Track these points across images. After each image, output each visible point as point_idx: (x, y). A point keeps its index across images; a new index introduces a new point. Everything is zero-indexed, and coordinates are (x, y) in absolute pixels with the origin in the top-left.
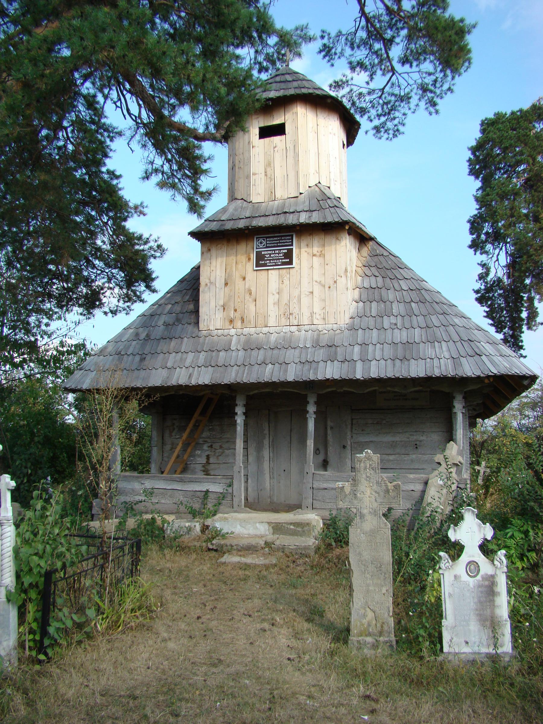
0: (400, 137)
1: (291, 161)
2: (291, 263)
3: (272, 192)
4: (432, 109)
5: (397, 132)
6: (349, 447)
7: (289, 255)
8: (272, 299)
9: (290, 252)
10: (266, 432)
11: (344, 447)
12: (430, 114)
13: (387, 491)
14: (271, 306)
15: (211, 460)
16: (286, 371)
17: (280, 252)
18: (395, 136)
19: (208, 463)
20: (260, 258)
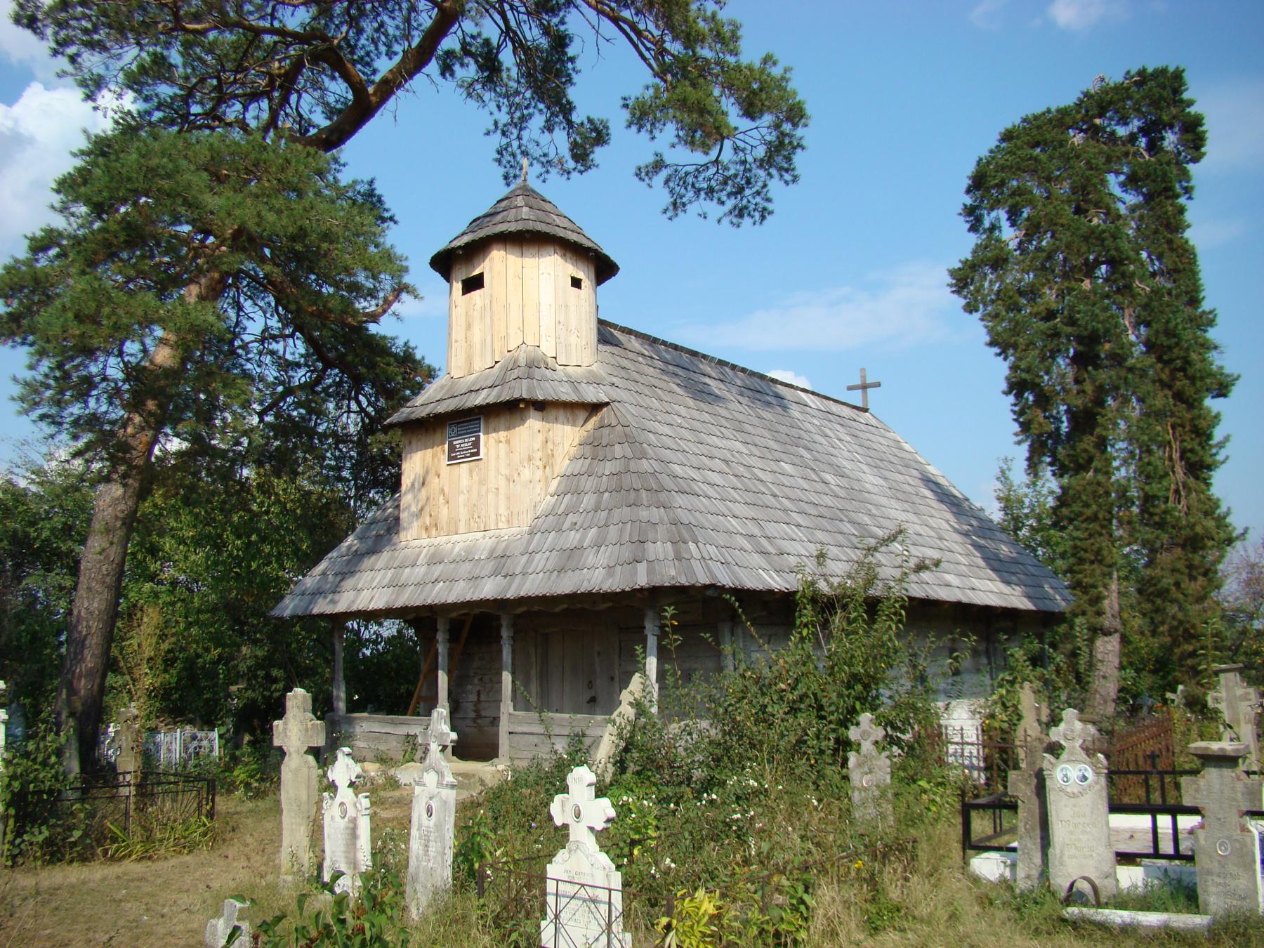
0: (769, 218)
1: (488, 320)
2: (477, 454)
3: (470, 364)
4: (787, 177)
5: (764, 214)
6: (617, 679)
7: (476, 444)
8: (462, 498)
9: (478, 438)
10: (533, 660)
11: (612, 679)
12: (787, 183)
13: (307, 730)
14: (462, 508)
15: (483, 698)
16: (635, 573)
17: (463, 443)
18: (763, 218)
19: (479, 701)
20: (452, 448)
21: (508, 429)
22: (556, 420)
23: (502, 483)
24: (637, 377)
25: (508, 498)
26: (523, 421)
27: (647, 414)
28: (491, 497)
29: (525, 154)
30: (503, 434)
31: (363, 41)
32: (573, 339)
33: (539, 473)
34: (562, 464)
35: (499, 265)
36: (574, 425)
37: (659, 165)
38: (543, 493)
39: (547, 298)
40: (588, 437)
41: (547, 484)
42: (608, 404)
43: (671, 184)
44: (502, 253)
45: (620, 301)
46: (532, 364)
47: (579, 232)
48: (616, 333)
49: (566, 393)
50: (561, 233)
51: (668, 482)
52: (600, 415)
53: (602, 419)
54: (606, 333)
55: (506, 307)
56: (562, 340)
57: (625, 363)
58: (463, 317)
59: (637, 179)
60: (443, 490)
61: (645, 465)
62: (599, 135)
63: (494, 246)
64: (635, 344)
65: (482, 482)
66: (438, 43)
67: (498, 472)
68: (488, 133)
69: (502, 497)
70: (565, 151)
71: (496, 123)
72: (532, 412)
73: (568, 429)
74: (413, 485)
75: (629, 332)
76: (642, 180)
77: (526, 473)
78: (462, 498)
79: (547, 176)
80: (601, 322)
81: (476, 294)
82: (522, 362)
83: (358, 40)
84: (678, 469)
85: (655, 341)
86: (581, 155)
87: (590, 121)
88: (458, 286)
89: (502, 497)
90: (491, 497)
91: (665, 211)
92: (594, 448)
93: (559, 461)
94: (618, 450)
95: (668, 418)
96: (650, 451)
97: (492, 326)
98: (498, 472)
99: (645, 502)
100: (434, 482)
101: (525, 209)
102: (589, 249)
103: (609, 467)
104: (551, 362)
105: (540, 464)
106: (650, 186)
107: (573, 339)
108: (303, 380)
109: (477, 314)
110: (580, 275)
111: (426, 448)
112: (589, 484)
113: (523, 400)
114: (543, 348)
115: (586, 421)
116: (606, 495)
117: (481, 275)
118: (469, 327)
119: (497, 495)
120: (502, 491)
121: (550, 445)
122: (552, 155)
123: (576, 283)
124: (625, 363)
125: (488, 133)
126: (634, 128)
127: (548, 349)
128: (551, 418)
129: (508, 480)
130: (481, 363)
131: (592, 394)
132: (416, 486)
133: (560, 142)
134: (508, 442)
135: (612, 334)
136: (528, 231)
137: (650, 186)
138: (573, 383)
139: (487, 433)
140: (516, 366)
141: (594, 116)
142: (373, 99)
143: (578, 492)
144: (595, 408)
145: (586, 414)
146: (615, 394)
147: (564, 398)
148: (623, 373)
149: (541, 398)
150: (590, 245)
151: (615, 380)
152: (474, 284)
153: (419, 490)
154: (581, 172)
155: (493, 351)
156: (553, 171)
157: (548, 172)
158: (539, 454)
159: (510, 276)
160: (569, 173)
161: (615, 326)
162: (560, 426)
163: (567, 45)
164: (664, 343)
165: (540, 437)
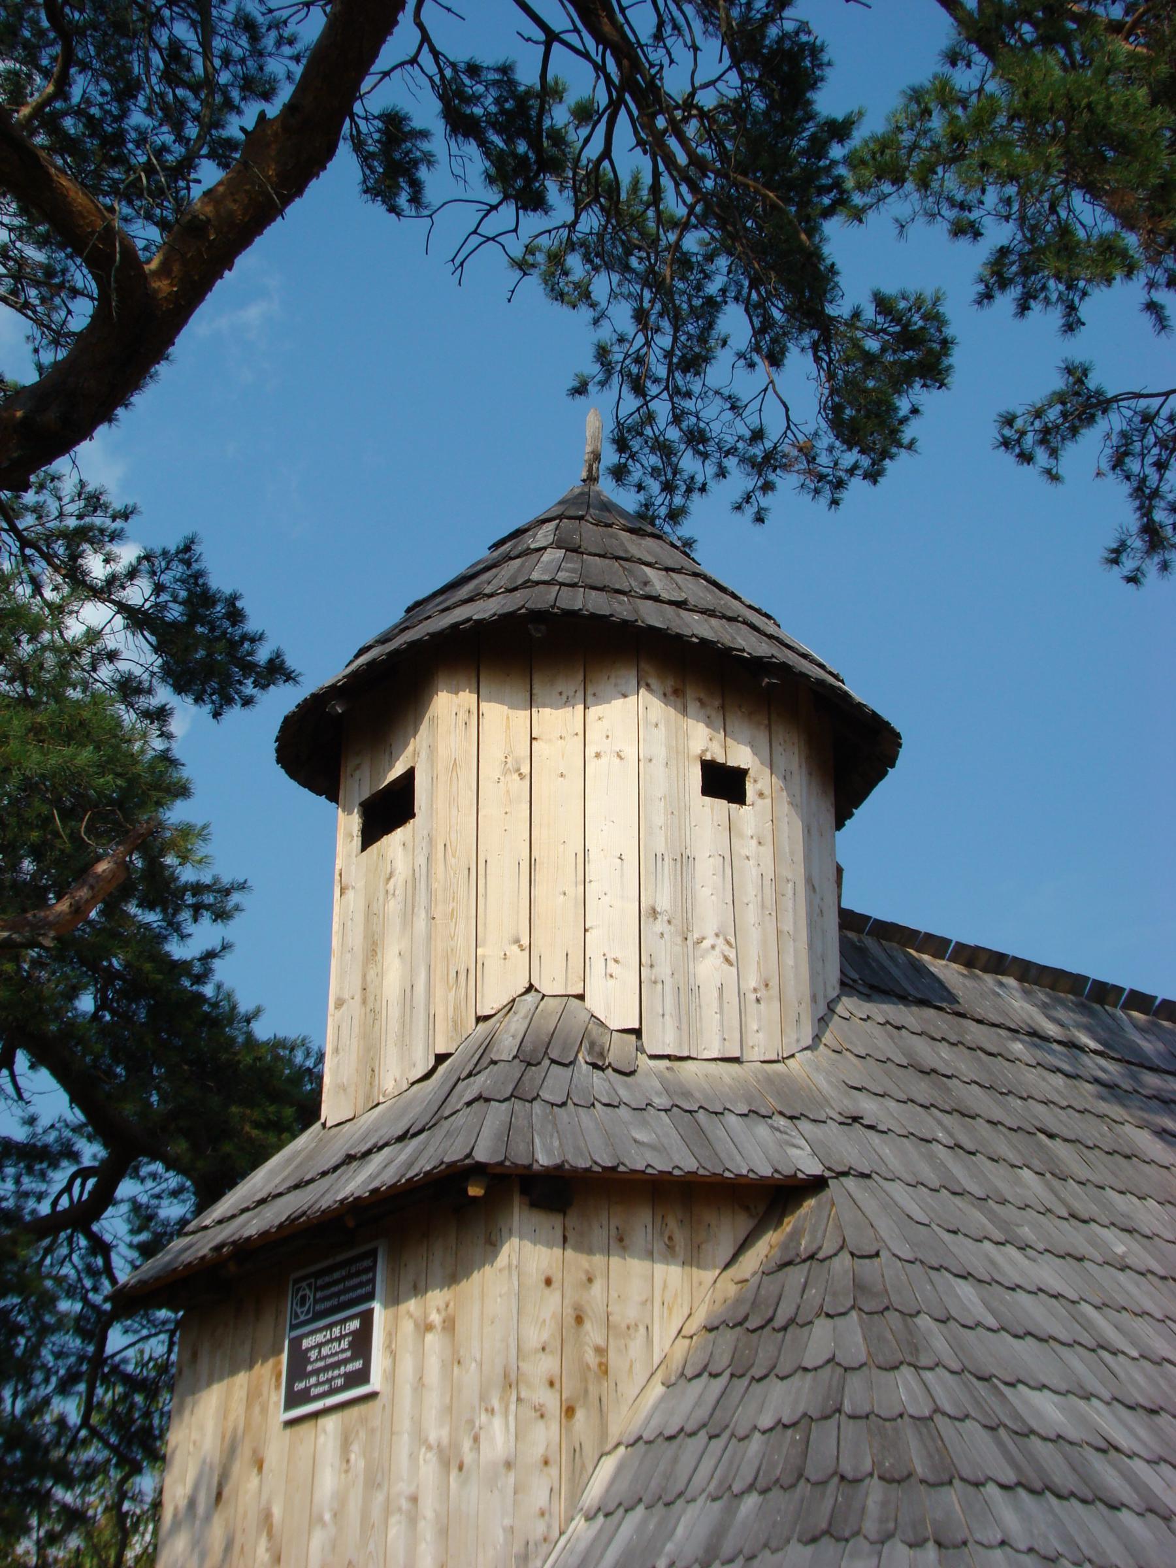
2: (362, 1377)
7: (361, 1343)
9: (367, 1318)
17: (325, 1342)
20: (298, 1367)
21: (453, 1278)
22: (621, 1243)
23: (429, 1468)
24: (976, 1099)
25: (444, 1532)
26: (493, 1245)
27: (977, 1219)
28: (396, 1529)
29: (697, 438)
30: (437, 1298)
31: (137, 118)
32: (709, 970)
33: (544, 1436)
34: (639, 1398)
35: (461, 736)
36: (693, 1258)
37: (1081, 404)
38: (560, 1508)
39: (613, 836)
40: (738, 1301)
41: (578, 1480)
42: (817, 1184)
43: (1134, 465)
44: (467, 698)
45: (912, 856)
46: (535, 1055)
47: (756, 620)
48: (941, 968)
49: (654, 1147)
50: (653, 616)
51: (978, 1450)
52: (790, 1223)
53: (795, 1235)
54: (873, 960)
55: (477, 869)
56: (663, 970)
57: (942, 1057)
58: (360, 918)
59: (1008, 459)
60: (267, 1516)
61: (904, 1391)
62: (917, 348)
63: (441, 681)
64: (1018, 1004)
65: (375, 1479)
66: (352, 93)
67: (419, 1438)
68: (580, 390)
69: (427, 1529)
70: (809, 415)
71: (602, 353)
72: (519, 1216)
73: (670, 1276)
74: (192, 1503)
75: (974, 958)
76: (1026, 458)
77: (498, 1437)
78: (318, 1540)
79: (765, 501)
80: (850, 921)
81: (395, 841)
82: (506, 1047)
83: (124, 114)
84: (1048, 1410)
85: (1095, 995)
86: (868, 424)
87: (883, 304)
88: (350, 823)
89: (427, 1529)
90: (396, 1529)
91: (1115, 556)
92: (747, 1339)
93: (630, 1390)
94: (820, 1341)
95: (1074, 1237)
96: (938, 1341)
97: (429, 938)
98: (419, 1438)
99: (871, 1527)
100: (247, 1488)
101: (553, 556)
102: (759, 665)
103: (779, 1401)
104: (619, 1050)
105: (551, 1401)
106: (1053, 476)
107: (709, 970)
108: (64, 1202)
109: (393, 906)
110: (740, 755)
111: (233, 1372)
112: (701, 1463)
113: (479, 1170)
114: (594, 1003)
115: (742, 1247)
116: (751, 1501)
117: (410, 775)
118: (373, 950)
119: (413, 1521)
120: (429, 1507)
121: (593, 1334)
122: (774, 431)
123: (723, 782)
124: (942, 1057)
125: (580, 390)
126: (1006, 301)
127: (613, 1003)
128: (599, 1234)
129: (445, 1463)
130: (398, 1070)
131: (756, 1152)
132: (201, 1509)
133: (796, 393)
134: (450, 1325)
135: (920, 970)
136: (538, 616)
137: (1053, 476)
138: (688, 1111)
139: (394, 1300)
140: (484, 1058)
141: (890, 289)
142: (162, 286)
143: (668, 1501)
144: (776, 1197)
145: (744, 1224)
146: (849, 1148)
147: (637, 1160)
148: (922, 1089)
149: (543, 1160)
150: (759, 648)
151: (868, 1107)
152: (389, 810)
153: (208, 1518)
154: (873, 476)
155: (431, 1019)
156: (787, 482)
157: (768, 487)
158: (547, 1365)
159: (491, 770)
160: (839, 484)
161: (937, 945)
162: (636, 1266)
163: (814, 83)
164: (1139, 1000)
165: (551, 1304)
